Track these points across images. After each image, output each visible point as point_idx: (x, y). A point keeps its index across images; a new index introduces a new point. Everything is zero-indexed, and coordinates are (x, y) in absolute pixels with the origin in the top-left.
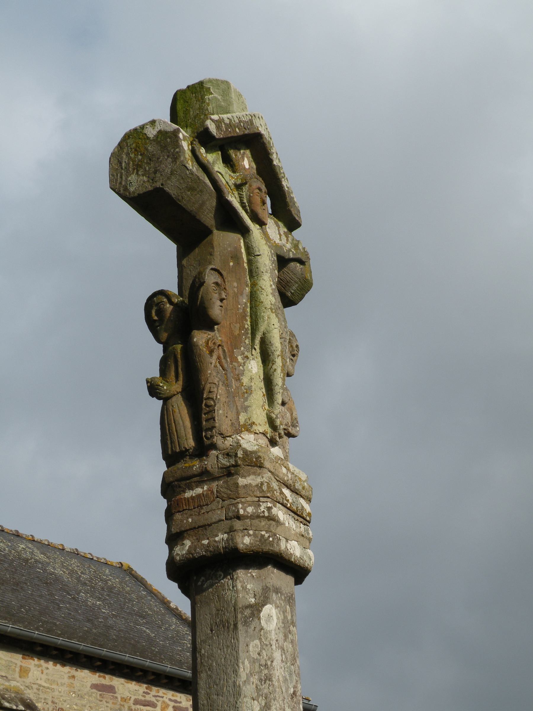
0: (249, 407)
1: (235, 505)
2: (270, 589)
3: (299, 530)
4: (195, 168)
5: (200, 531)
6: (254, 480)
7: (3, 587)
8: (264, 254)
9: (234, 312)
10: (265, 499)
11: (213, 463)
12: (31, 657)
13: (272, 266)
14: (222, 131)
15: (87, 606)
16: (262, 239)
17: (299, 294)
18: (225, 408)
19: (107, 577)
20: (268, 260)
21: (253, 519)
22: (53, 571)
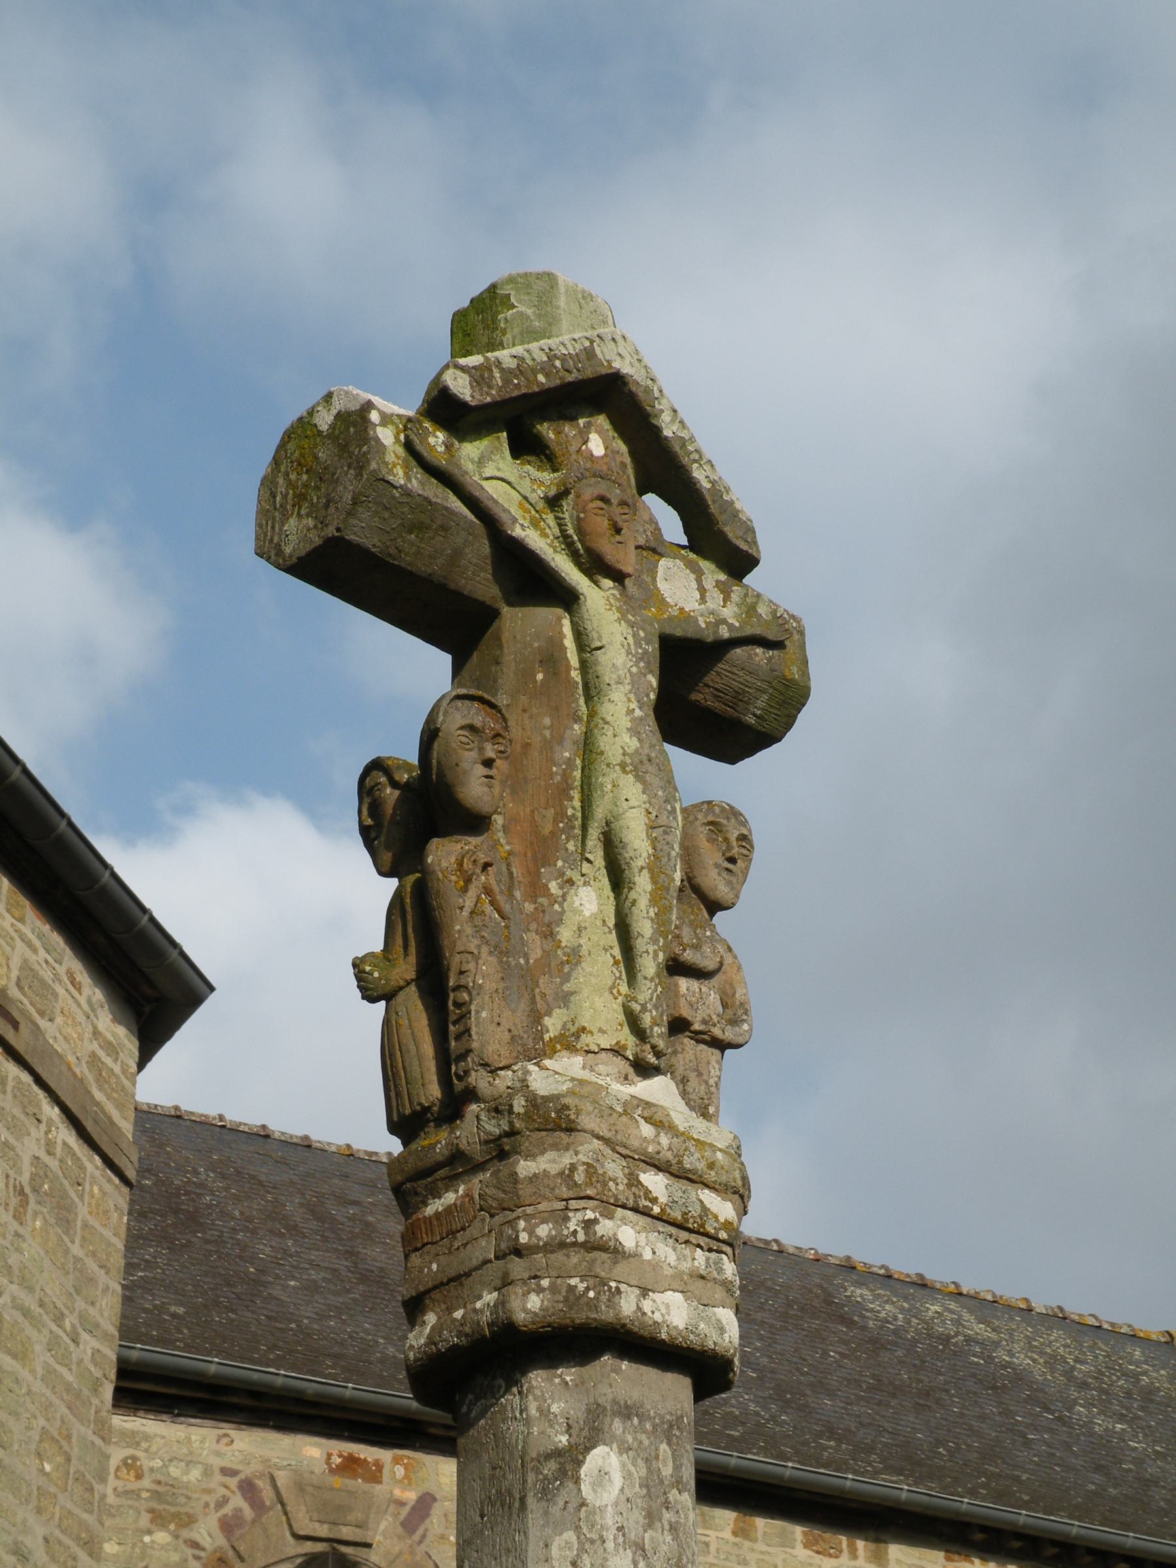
0: (572, 993)
1: (512, 1223)
2: (605, 1409)
3: (689, 1266)
4: (414, 481)
5: (452, 1289)
6: (554, 1161)
7: (896, 1402)
8: (611, 643)
9: (543, 783)
10: (582, 1203)
11: (471, 1133)
12: (966, 1556)
13: (639, 667)
14: (490, 387)
15: (1092, 1434)
16: (610, 609)
17: (778, 715)
18: (495, 1004)
19: (1137, 1367)
20: (624, 655)
21: (552, 1252)
22: (1007, 1359)
